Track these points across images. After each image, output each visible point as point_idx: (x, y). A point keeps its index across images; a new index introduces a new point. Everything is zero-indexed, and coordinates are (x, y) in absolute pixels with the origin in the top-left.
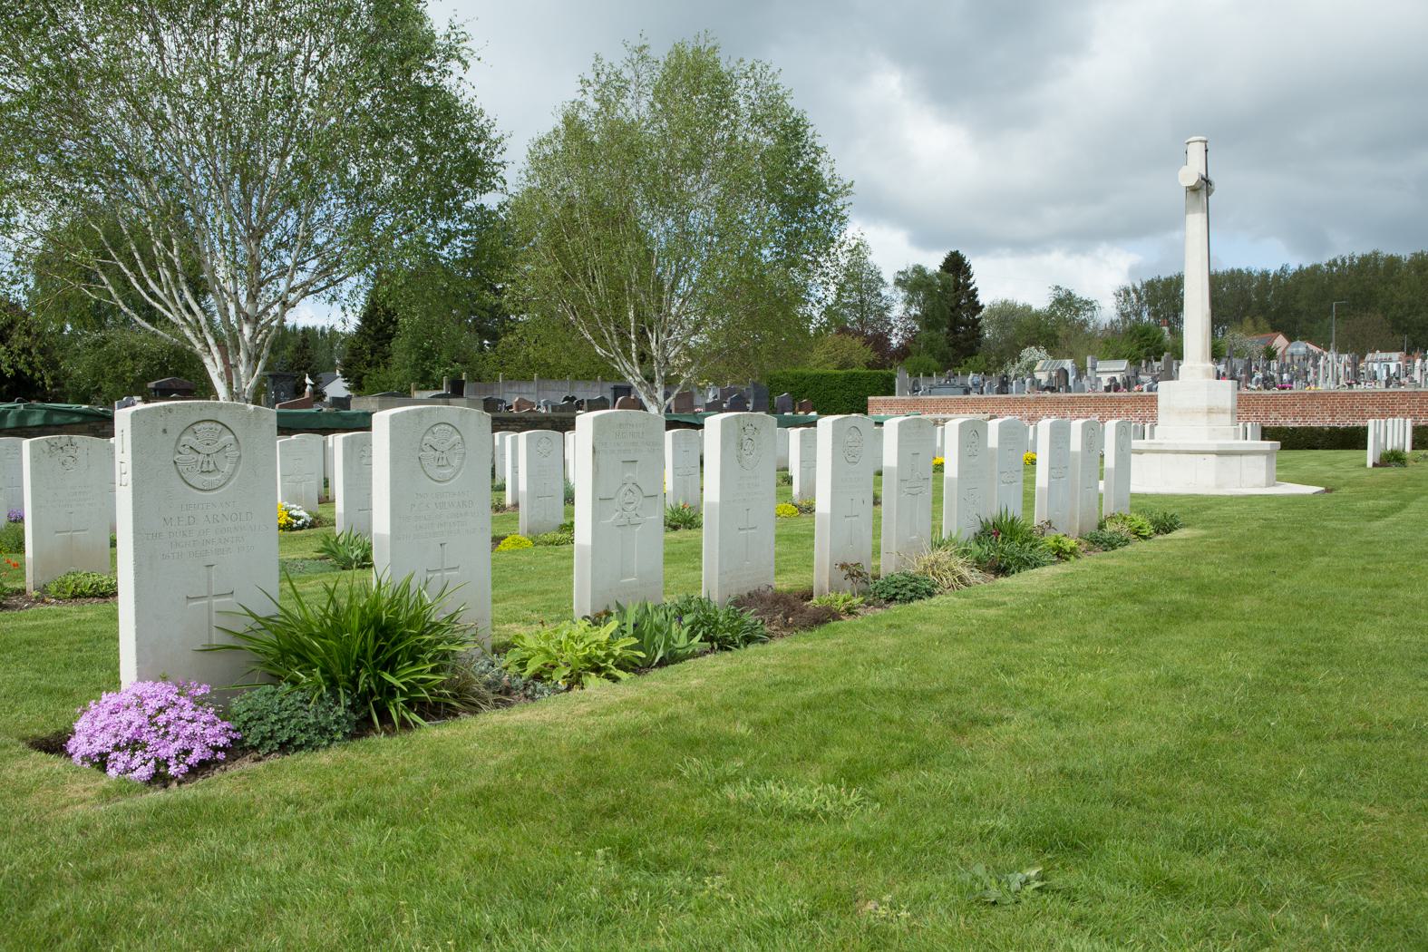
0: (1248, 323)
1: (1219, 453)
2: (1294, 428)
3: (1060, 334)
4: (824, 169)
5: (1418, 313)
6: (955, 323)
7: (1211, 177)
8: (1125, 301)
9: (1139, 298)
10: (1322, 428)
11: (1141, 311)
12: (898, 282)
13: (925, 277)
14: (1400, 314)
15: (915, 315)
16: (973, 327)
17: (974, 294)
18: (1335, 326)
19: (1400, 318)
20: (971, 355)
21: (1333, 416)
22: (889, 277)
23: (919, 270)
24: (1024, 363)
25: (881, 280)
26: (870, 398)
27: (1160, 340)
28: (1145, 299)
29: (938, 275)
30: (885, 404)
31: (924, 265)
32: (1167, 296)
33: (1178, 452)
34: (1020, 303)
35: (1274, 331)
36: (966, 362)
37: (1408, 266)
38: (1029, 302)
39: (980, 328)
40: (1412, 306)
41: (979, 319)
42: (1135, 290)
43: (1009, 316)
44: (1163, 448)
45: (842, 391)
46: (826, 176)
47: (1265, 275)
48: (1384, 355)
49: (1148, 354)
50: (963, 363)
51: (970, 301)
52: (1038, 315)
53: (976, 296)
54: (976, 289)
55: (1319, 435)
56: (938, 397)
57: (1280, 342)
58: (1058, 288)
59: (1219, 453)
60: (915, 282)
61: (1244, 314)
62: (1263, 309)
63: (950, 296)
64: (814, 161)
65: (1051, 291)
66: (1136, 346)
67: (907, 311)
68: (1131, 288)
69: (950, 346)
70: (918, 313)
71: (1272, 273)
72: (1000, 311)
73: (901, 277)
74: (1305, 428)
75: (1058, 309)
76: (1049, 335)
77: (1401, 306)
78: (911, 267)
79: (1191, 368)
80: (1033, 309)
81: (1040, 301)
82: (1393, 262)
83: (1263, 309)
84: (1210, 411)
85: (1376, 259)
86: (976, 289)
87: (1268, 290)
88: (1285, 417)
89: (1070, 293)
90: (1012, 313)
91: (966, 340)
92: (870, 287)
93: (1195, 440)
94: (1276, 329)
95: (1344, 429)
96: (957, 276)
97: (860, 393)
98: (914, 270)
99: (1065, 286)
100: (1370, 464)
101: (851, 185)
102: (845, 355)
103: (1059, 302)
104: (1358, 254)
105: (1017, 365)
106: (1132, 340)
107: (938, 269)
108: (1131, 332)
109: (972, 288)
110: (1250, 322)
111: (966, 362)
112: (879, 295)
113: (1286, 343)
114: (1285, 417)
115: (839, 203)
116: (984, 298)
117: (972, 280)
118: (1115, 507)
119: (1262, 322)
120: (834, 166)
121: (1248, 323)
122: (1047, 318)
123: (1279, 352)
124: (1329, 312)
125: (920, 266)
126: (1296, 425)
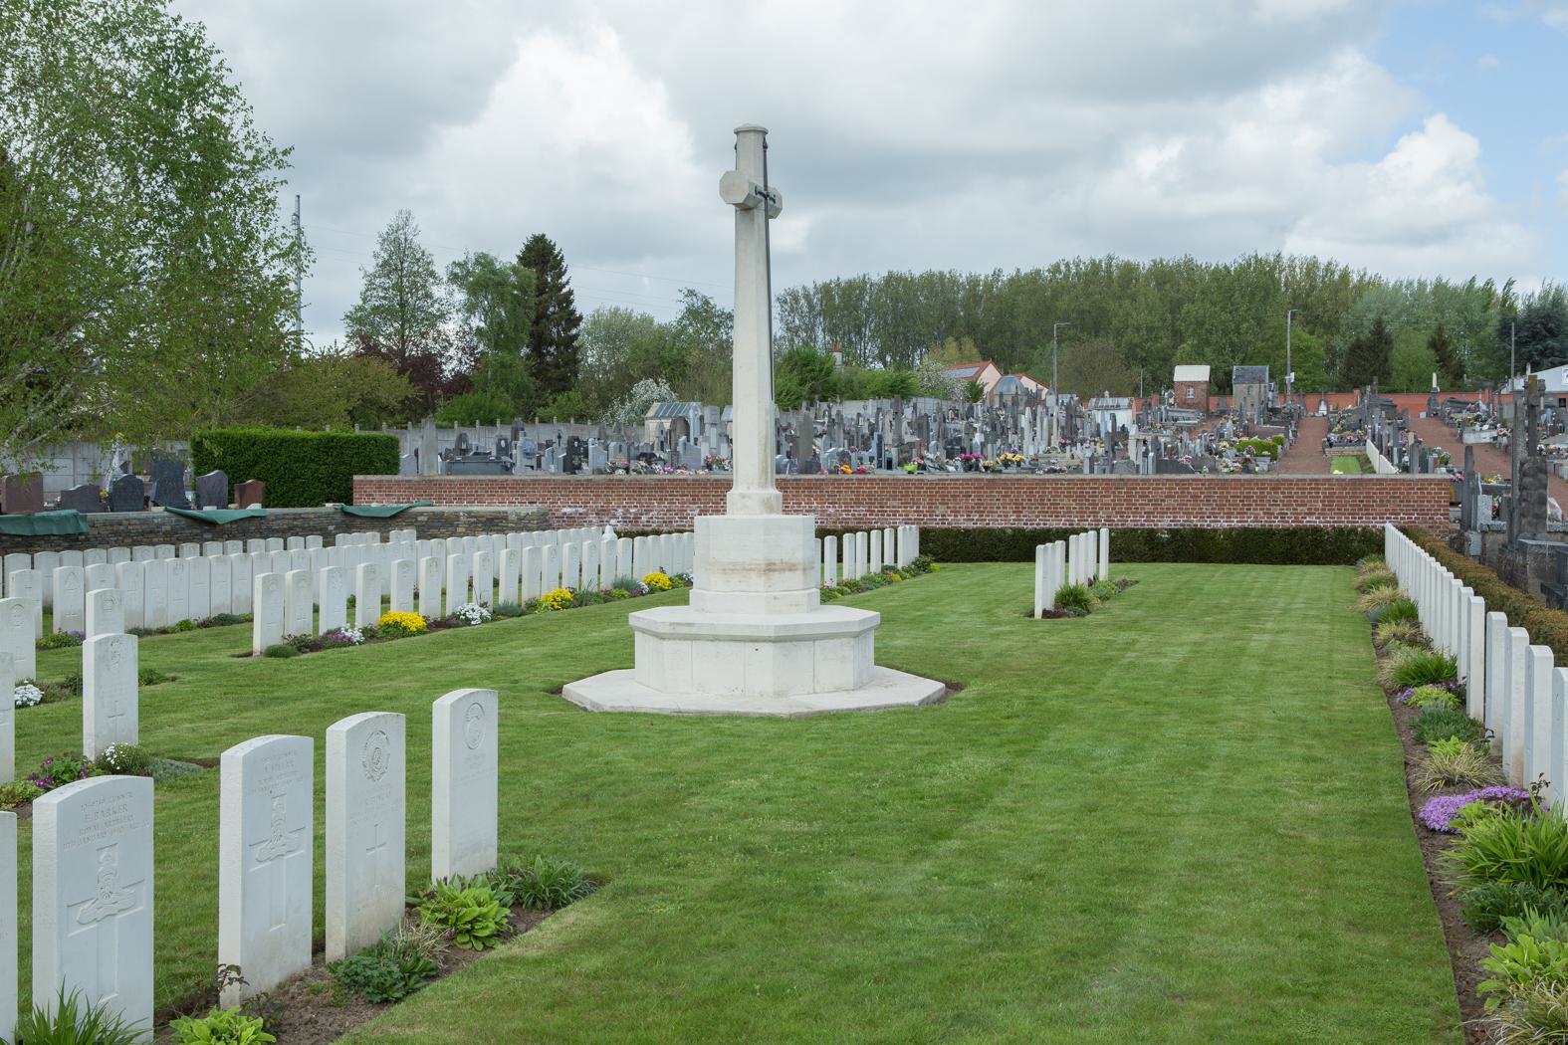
0: (951, 346)
1: (776, 640)
2: (967, 531)
3: (690, 360)
4: (235, 123)
5: (1157, 339)
6: (539, 342)
7: (773, 184)
8: (792, 311)
9: (811, 306)
10: (1003, 530)
11: (814, 325)
12: (454, 278)
13: (494, 272)
14: (1136, 340)
15: (479, 329)
16: (567, 348)
17: (567, 299)
18: (1057, 355)
19: (1136, 346)
20: (564, 389)
21: (1018, 512)
22: (441, 269)
23: (484, 261)
24: (637, 402)
25: (432, 274)
26: (355, 477)
27: (829, 373)
28: (818, 308)
29: (514, 269)
30: (379, 486)
31: (492, 254)
32: (846, 307)
33: (715, 639)
34: (636, 314)
35: (984, 360)
36: (555, 400)
37: (1146, 277)
38: (650, 312)
39: (576, 350)
40: (1150, 330)
41: (576, 337)
42: (807, 297)
43: (618, 330)
44: (693, 631)
45: (313, 466)
46: (238, 133)
47: (974, 282)
48: (1110, 401)
49: (813, 391)
50: (550, 401)
51: (562, 309)
52: (663, 331)
53: (571, 302)
54: (571, 293)
55: (1000, 540)
56: (461, 477)
57: (990, 376)
58: (691, 293)
59: (776, 640)
60: (480, 280)
61: (948, 331)
62: (972, 328)
63: (533, 301)
64: (220, 109)
65: (681, 296)
66: (796, 380)
67: (466, 321)
68: (801, 292)
69: (532, 375)
70: (482, 325)
71: (982, 278)
72: (608, 326)
73: (457, 270)
74: (981, 531)
75: (691, 324)
76: (676, 361)
77: (1138, 329)
78: (472, 257)
79: (743, 496)
80: (655, 323)
81: (667, 313)
82: (1129, 270)
83: (972, 328)
84: (770, 568)
85: (1109, 265)
86: (571, 293)
87: (977, 303)
88: (955, 512)
89: (707, 303)
90: (624, 330)
91: (557, 366)
92: (415, 283)
93: (750, 622)
94: (987, 355)
95: (1031, 531)
96: (542, 272)
97: (342, 468)
98: (477, 262)
99: (702, 291)
100: (1038, 612)
101: (285, 153)
102: (366, 389)
103: (692, 313)
104: (1086, 259)
105: (628, 405)
106: (791, 371)
107: (515, 261)
108: (790, 358)
109: (564, 290)
110: (954, 344)
111: (555, 400)
112: (428, 296)
113: (998, 375)
114: (955, 512)
115: (264, 176)
116: (582, 306)
117: (564, 279)
118: (453, 862)
119: (968, 344)
120: (251, 116)
121: (951, 346)
122: (676, 337)
123: (987, 389)
124: (1048, 336)
125: (485, 256)
126: (970, 525)
